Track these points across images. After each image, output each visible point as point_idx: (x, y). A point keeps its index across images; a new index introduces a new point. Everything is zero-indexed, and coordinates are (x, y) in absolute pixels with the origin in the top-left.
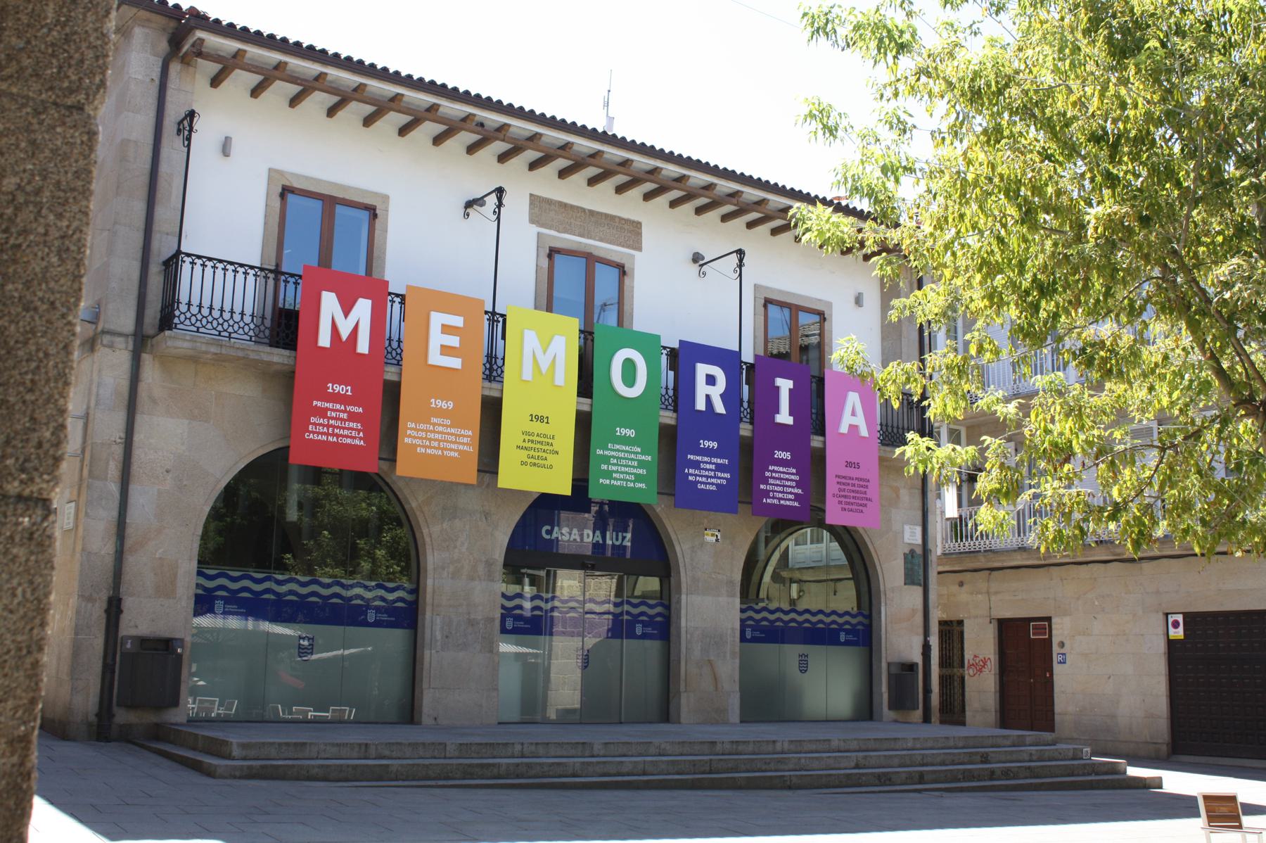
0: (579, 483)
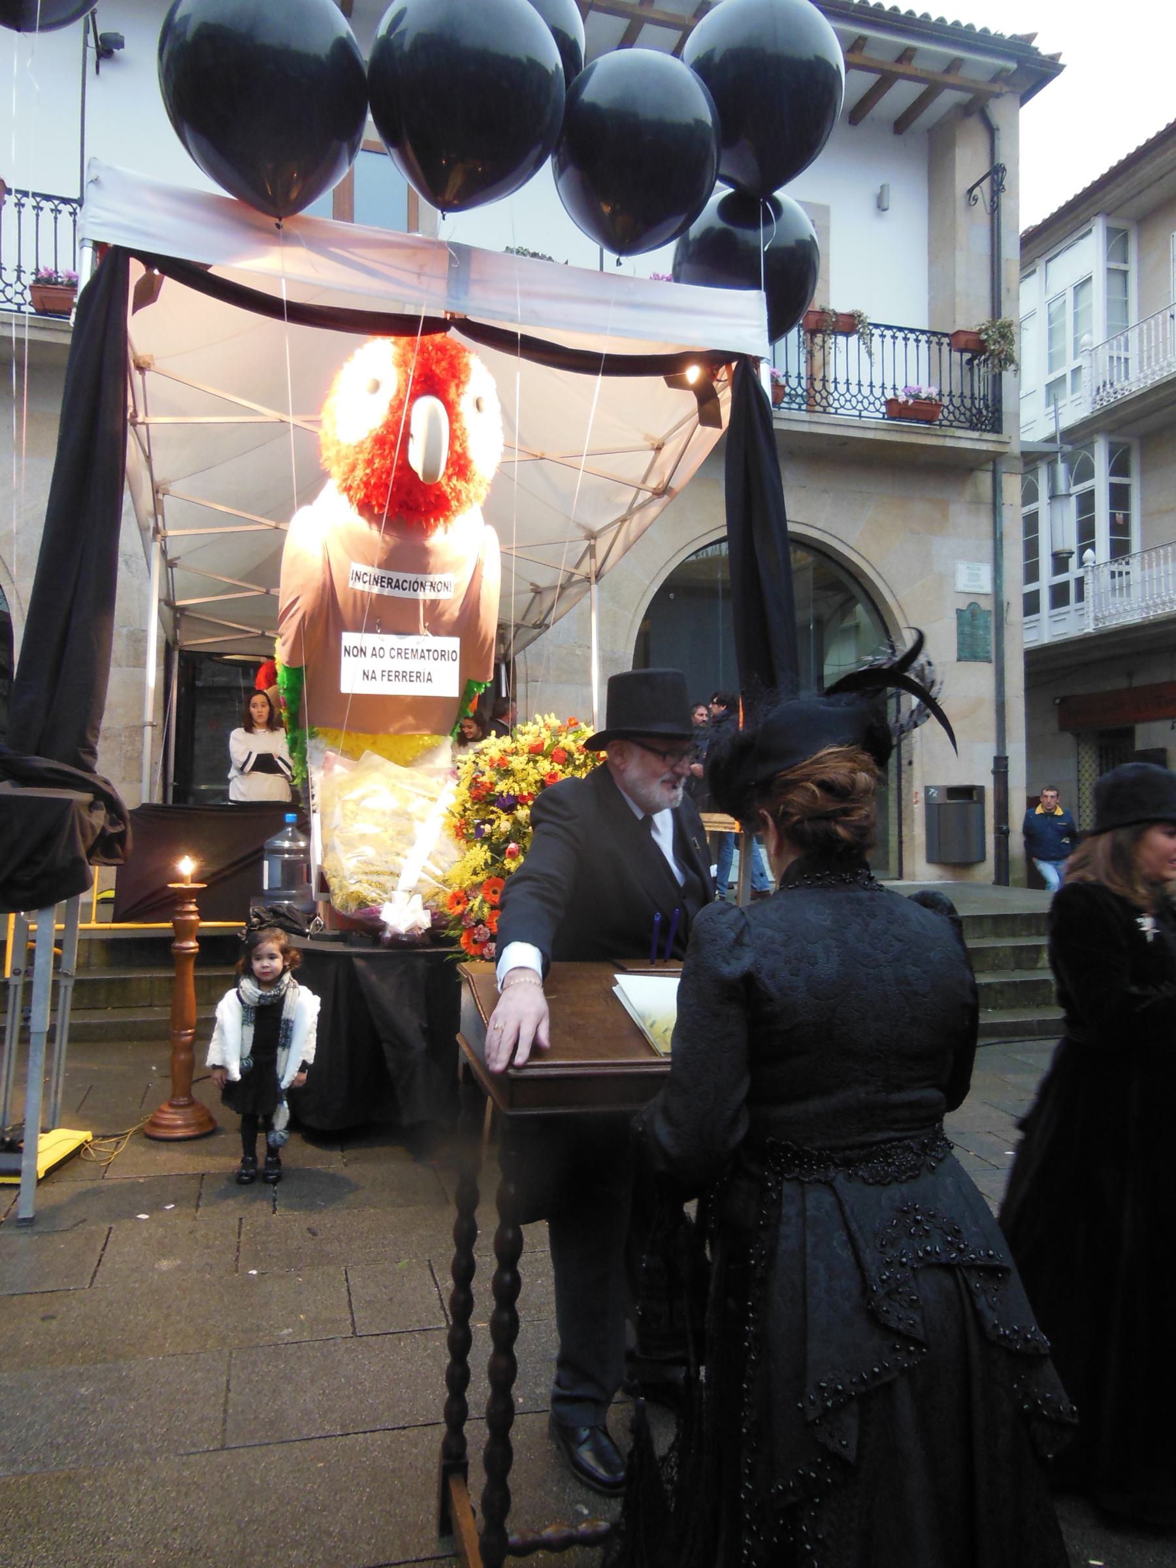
0: (412, 577)
